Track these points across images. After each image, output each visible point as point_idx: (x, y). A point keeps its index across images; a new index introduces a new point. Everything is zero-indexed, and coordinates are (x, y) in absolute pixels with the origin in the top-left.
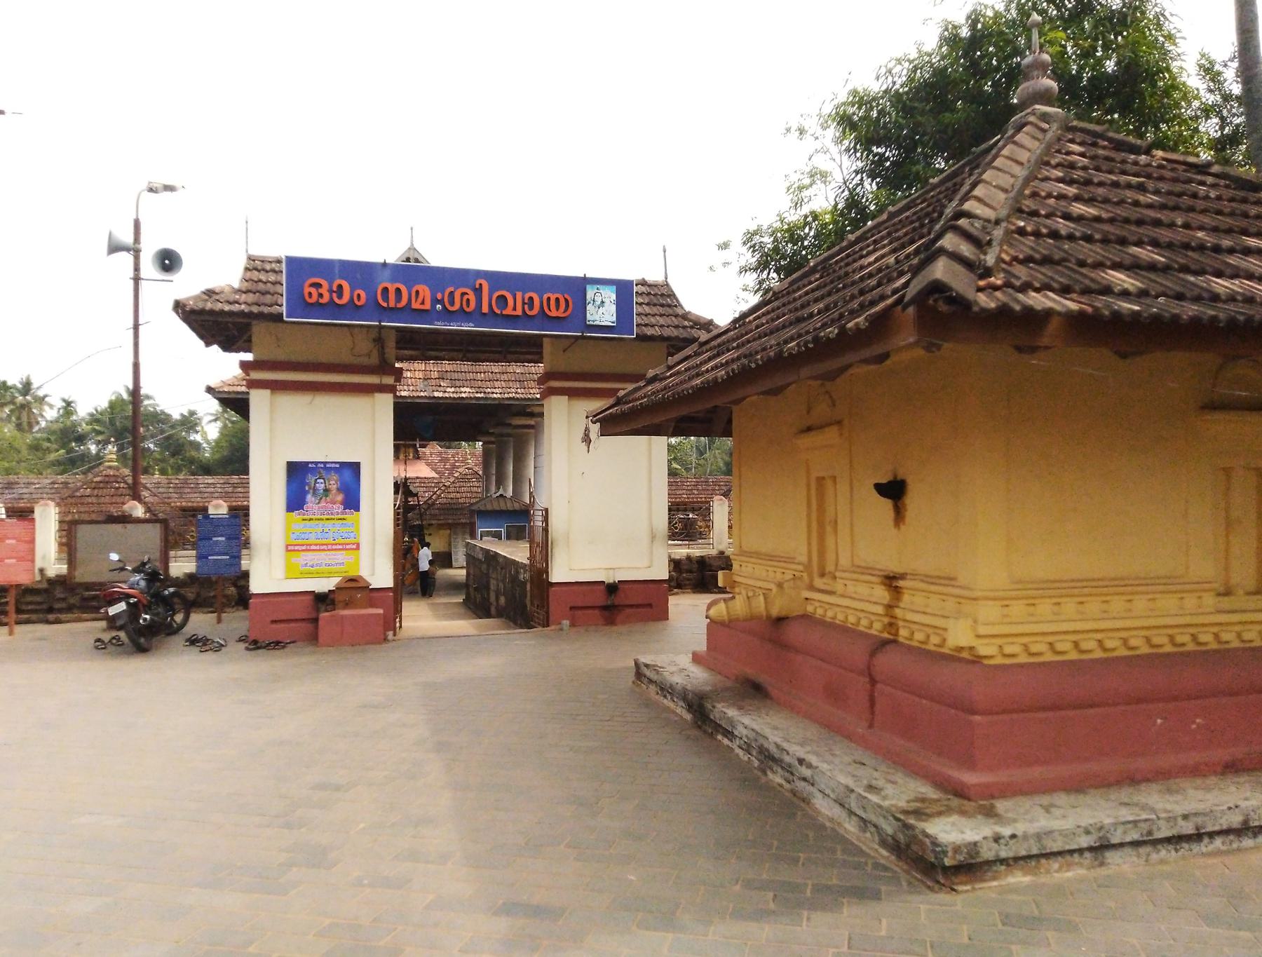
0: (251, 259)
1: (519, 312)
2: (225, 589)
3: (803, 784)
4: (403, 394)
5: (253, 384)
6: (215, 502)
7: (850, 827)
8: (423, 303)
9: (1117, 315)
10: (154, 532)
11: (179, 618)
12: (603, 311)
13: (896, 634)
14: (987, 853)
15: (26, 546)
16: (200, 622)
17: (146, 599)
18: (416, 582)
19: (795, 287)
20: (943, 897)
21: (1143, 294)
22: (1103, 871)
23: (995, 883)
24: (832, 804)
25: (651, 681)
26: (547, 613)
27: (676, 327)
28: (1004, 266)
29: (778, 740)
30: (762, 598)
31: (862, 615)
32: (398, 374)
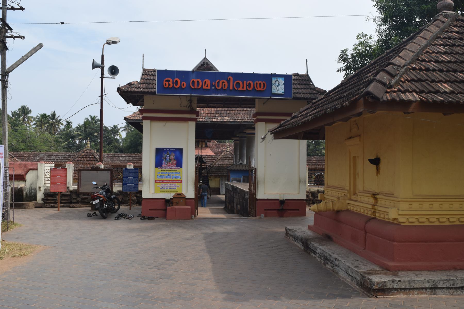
0: (144, 70)
1: (245, 89)
2: (133, 197)
3: (336, 267)
4: (201, 120)
5: (144, 118)
6: (129, 163)
7: (349, 280)
8: (207, 86)
9: (435, 102)
10: (107, 175)
11: (116, 207)
12: (279, 88)
13: (375, 216)
14: (389, 286)
15: (64, 178)
16: (123, 209)
17: (105, 199)
18: (200, 199)
19: (350, 81)
20: (372, 299)
21: (452, 92)
22: (433, 296)
23: (392, 296)
24: (344, 272)
25: (291, 236)
26: (256, 211)
27: (310, 94)
28: (401, 83)
29: (330, 253)
30: (331, 203)
31: (365, 209)
32: (198, 114)
